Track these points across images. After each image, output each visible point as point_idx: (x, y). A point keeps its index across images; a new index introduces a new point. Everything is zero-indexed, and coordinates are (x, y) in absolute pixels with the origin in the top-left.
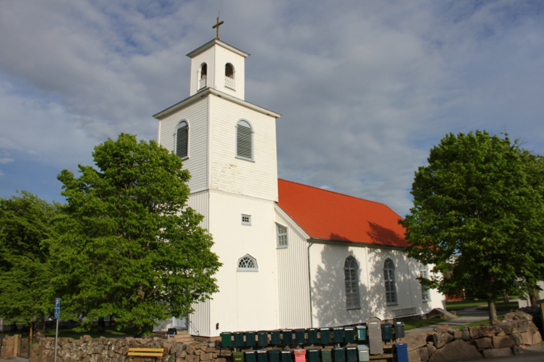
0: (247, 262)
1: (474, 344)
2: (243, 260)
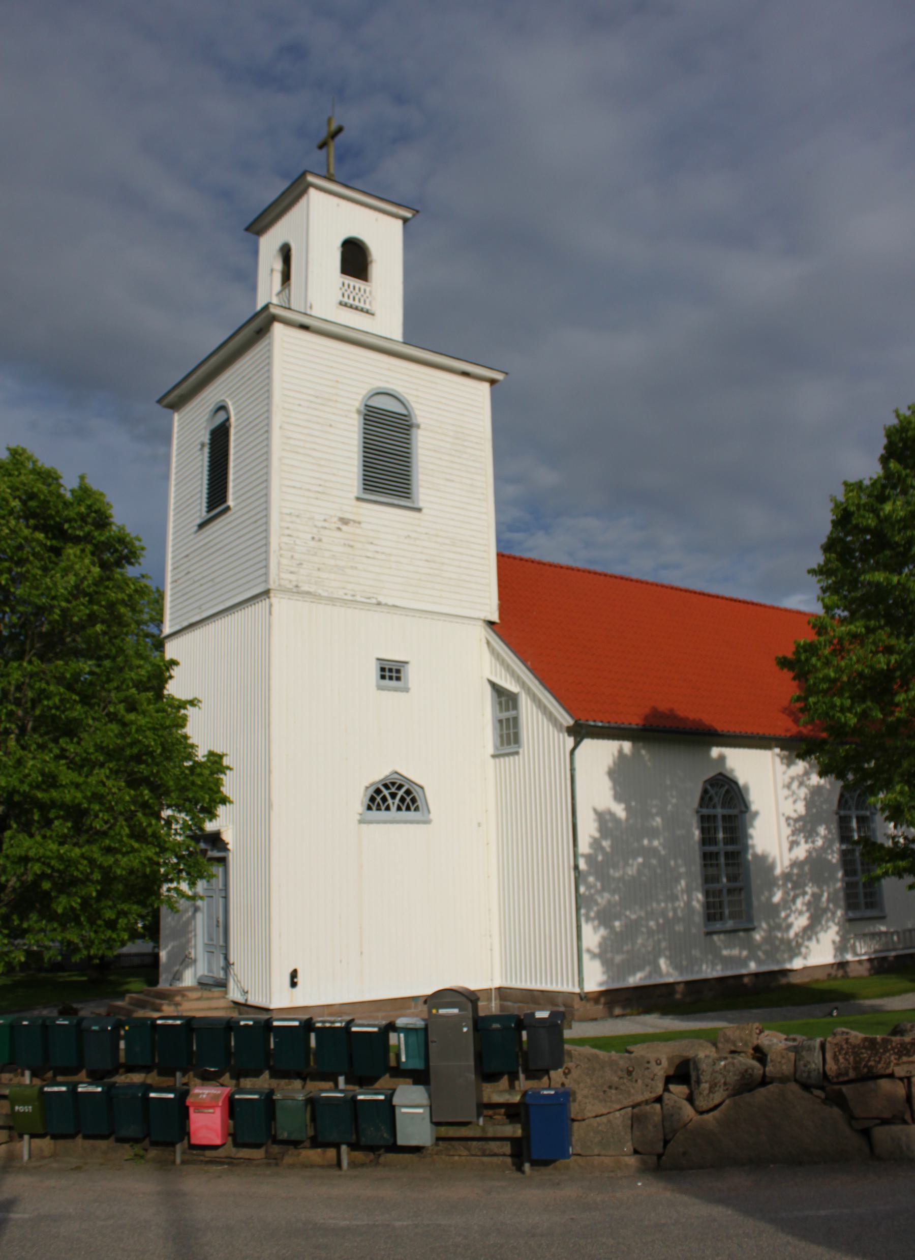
0: (393, 796)
1: (838, 1100)
2: (383, 789)
